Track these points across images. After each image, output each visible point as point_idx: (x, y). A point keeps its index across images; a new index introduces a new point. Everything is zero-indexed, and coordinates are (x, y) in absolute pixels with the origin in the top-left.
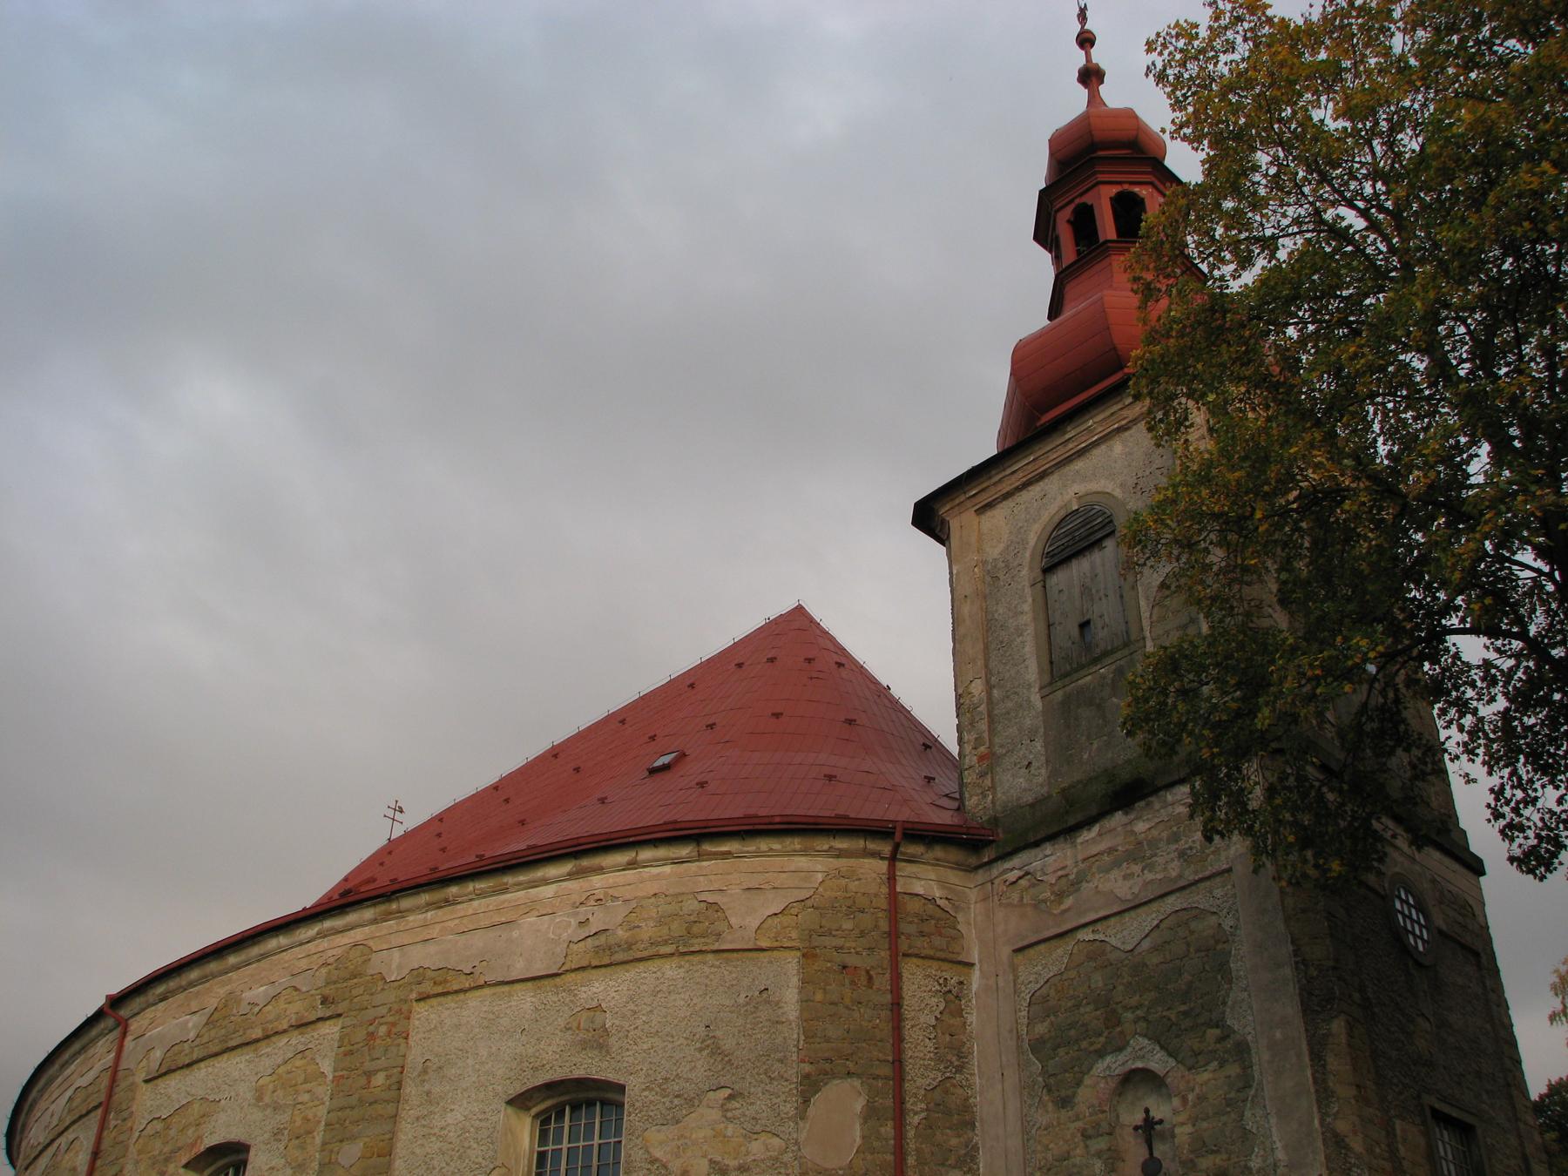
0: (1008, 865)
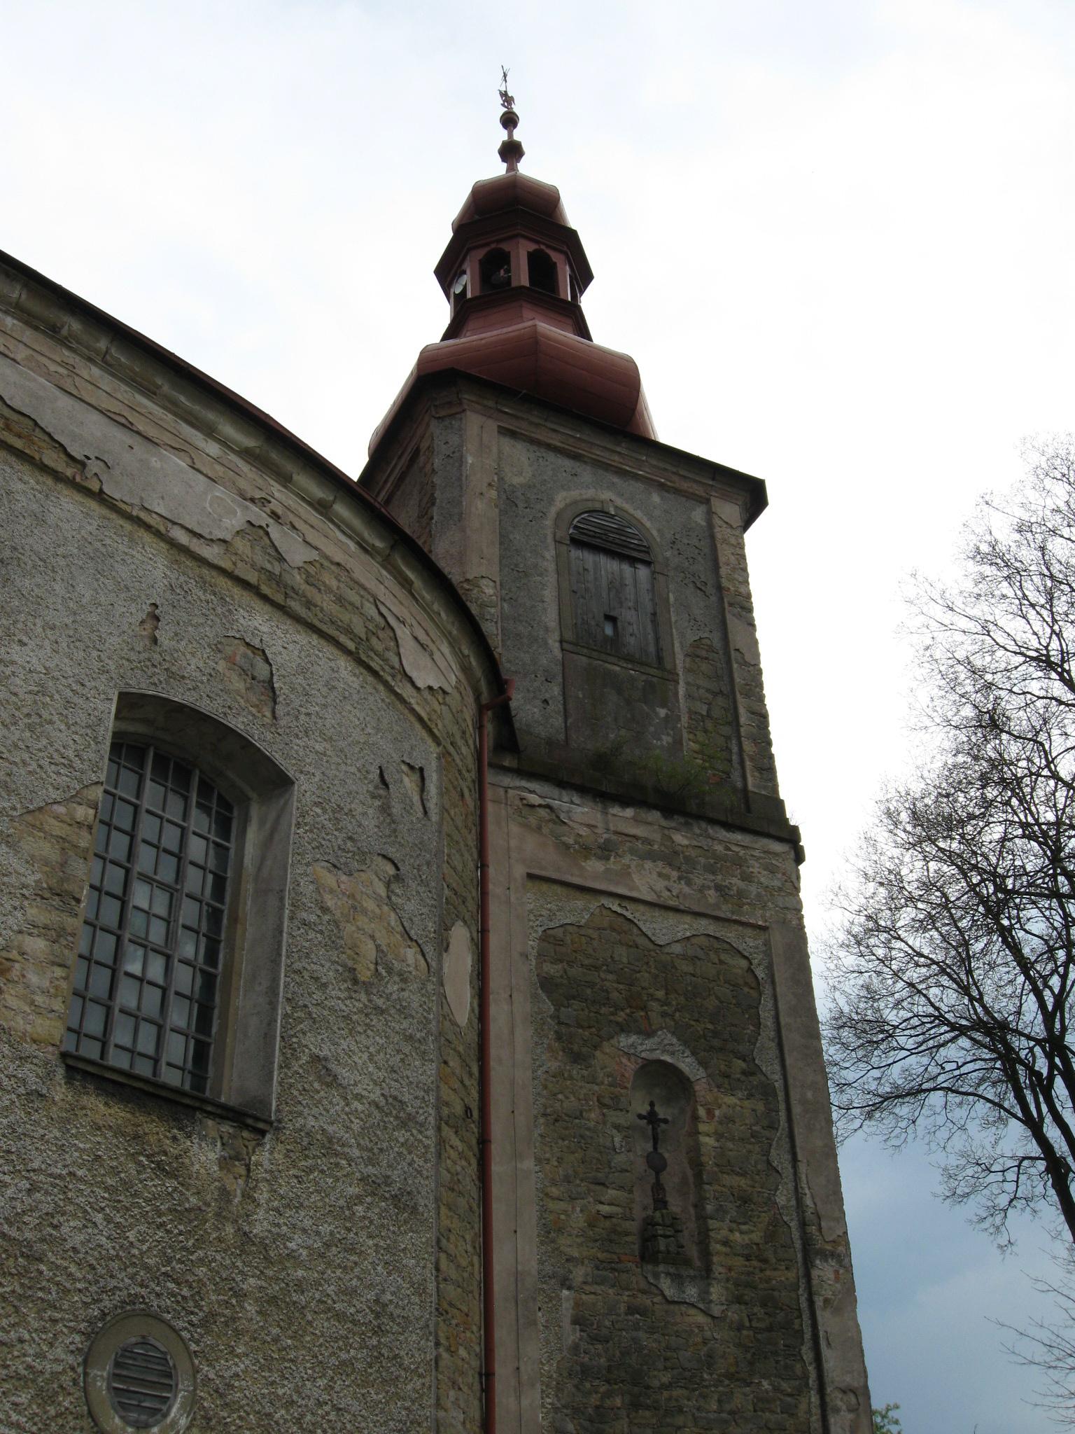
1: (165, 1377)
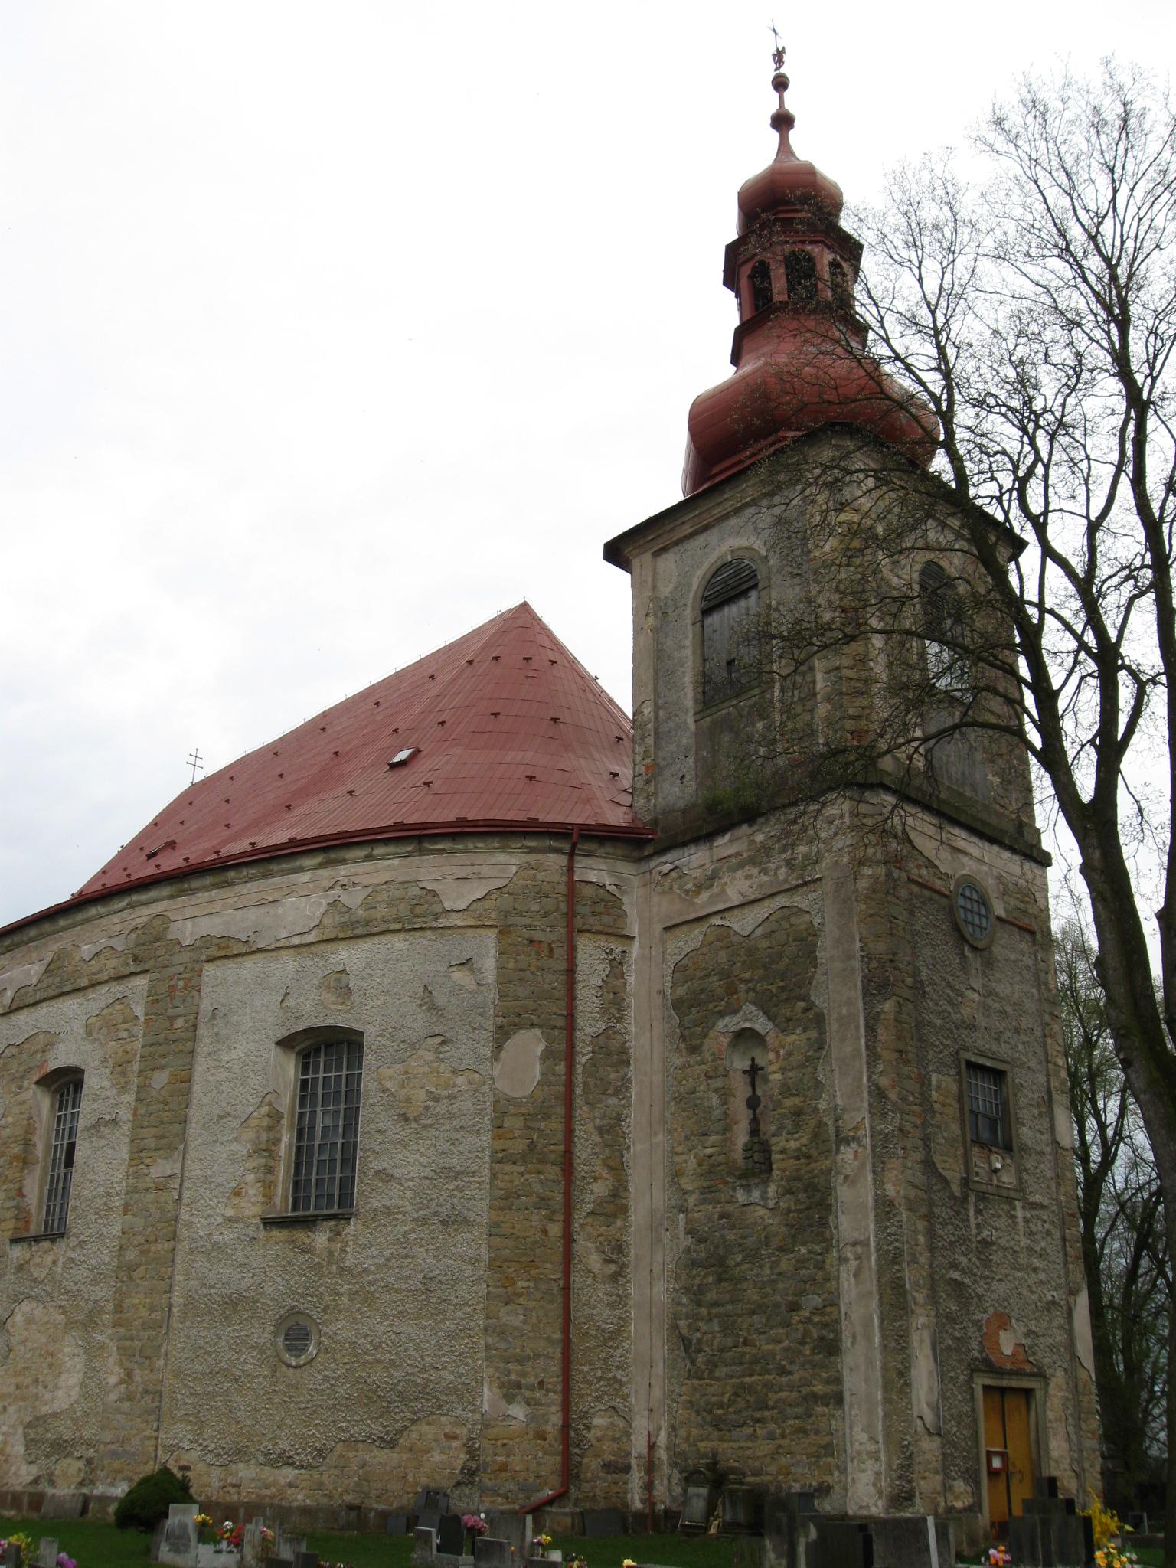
0: (663, 859)
1: (306, 1337)
